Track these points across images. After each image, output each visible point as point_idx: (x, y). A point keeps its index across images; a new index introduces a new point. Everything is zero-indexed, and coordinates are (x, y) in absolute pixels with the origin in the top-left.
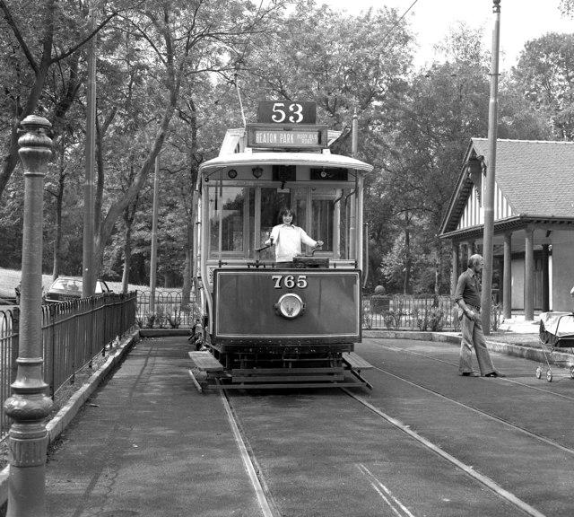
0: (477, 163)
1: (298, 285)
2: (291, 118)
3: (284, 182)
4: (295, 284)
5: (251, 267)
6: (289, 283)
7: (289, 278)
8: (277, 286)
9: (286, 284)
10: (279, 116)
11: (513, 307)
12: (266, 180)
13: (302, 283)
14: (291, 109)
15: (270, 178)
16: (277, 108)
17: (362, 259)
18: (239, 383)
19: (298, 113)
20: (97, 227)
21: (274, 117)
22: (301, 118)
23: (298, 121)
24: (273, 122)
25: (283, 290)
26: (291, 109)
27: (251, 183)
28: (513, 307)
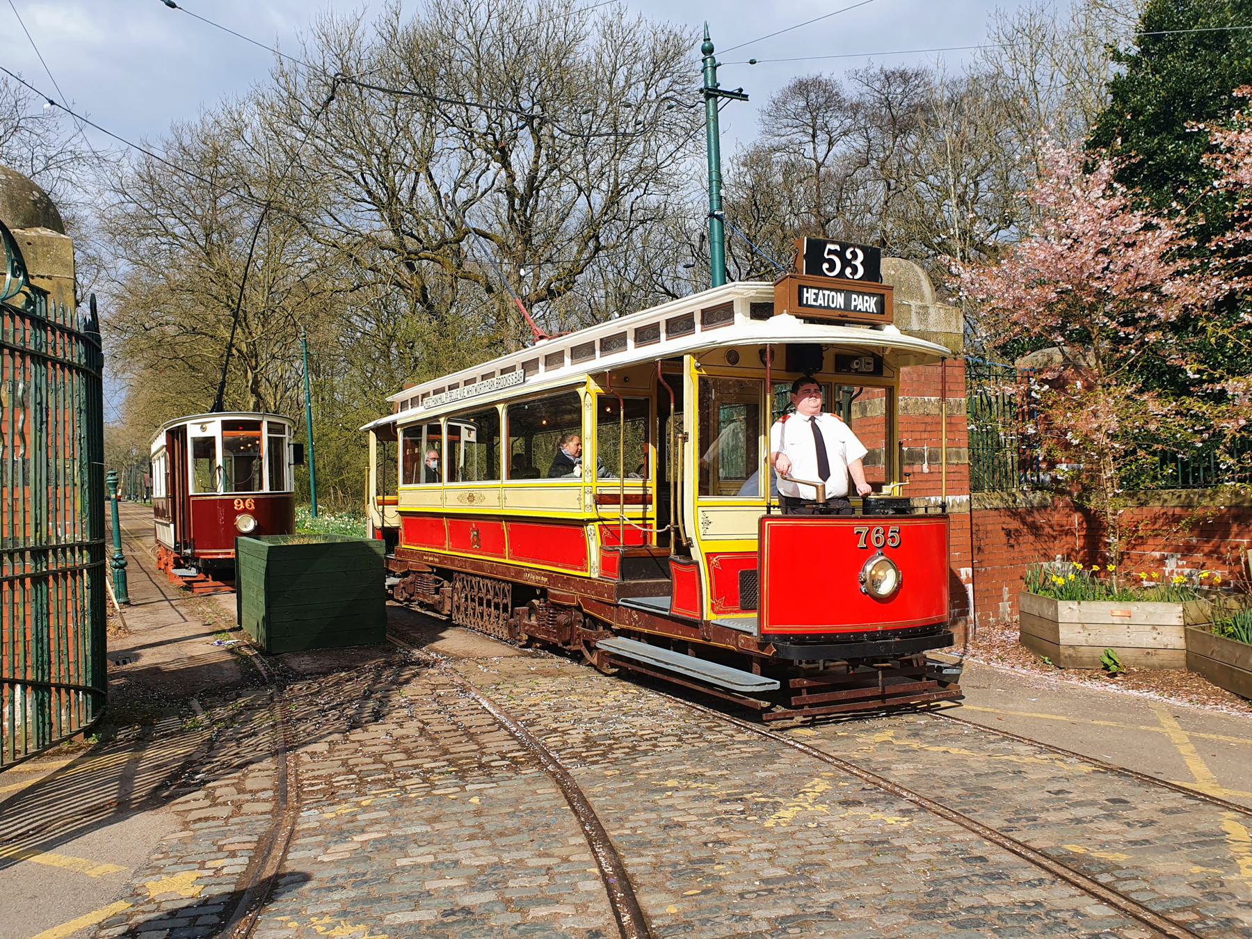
2: (848, 271)
7: (878, 532)
10: (832, 267)
14: (849, 256)
16: (830, 252)
19: (858, 263)
21: (826, 266)
25: (868, 552)
26: (849, 256)
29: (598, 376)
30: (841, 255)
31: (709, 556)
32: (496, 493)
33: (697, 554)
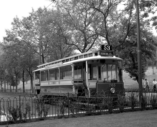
2: (108, 49)
6: (112, 86)
10: (105, 48)
14: (108, 47)
16: (105, 47)
19: (109, 48)
21: (104, 48)
25: (111, 87)
26: (108, 47)
29: (74, 63)
30: (107, 47)
31: (90, 89)
32: (58, 82)
33: (88, 89)
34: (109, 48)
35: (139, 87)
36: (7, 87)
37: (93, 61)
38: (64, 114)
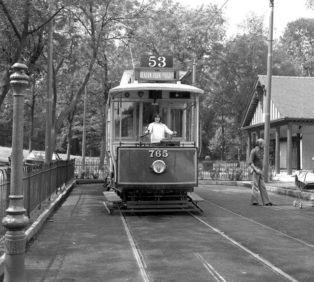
0: (261, 89)
1: (163, 155)
2: (159, 65)
3: (155, 99)
4: (162, 155)
5: (137, 145)
6: (158, 155)
7: (158, 152)
8: (152, 156)
9: (157, 155)
10: (153, 63)
11: (281, 167)
12: (146, 98)
13: (165, 154)
14: (159, 59)
15: (148, 97)
16: (151, 59)
17: (198, 141)
18: (131, 209)
19: (163, 61)
20: (53, 124)
21: (150, 64)
22: (165, 64)
23: (163, 66)
24: (150, 67)
25: (155, 158)
26: (159, 59)
27: (137, 100)
28: (281, 167)
34: (163, 61)
35: (97, 158)
36: (69, 198)
37: (127, 95)
38: (208, 98)
